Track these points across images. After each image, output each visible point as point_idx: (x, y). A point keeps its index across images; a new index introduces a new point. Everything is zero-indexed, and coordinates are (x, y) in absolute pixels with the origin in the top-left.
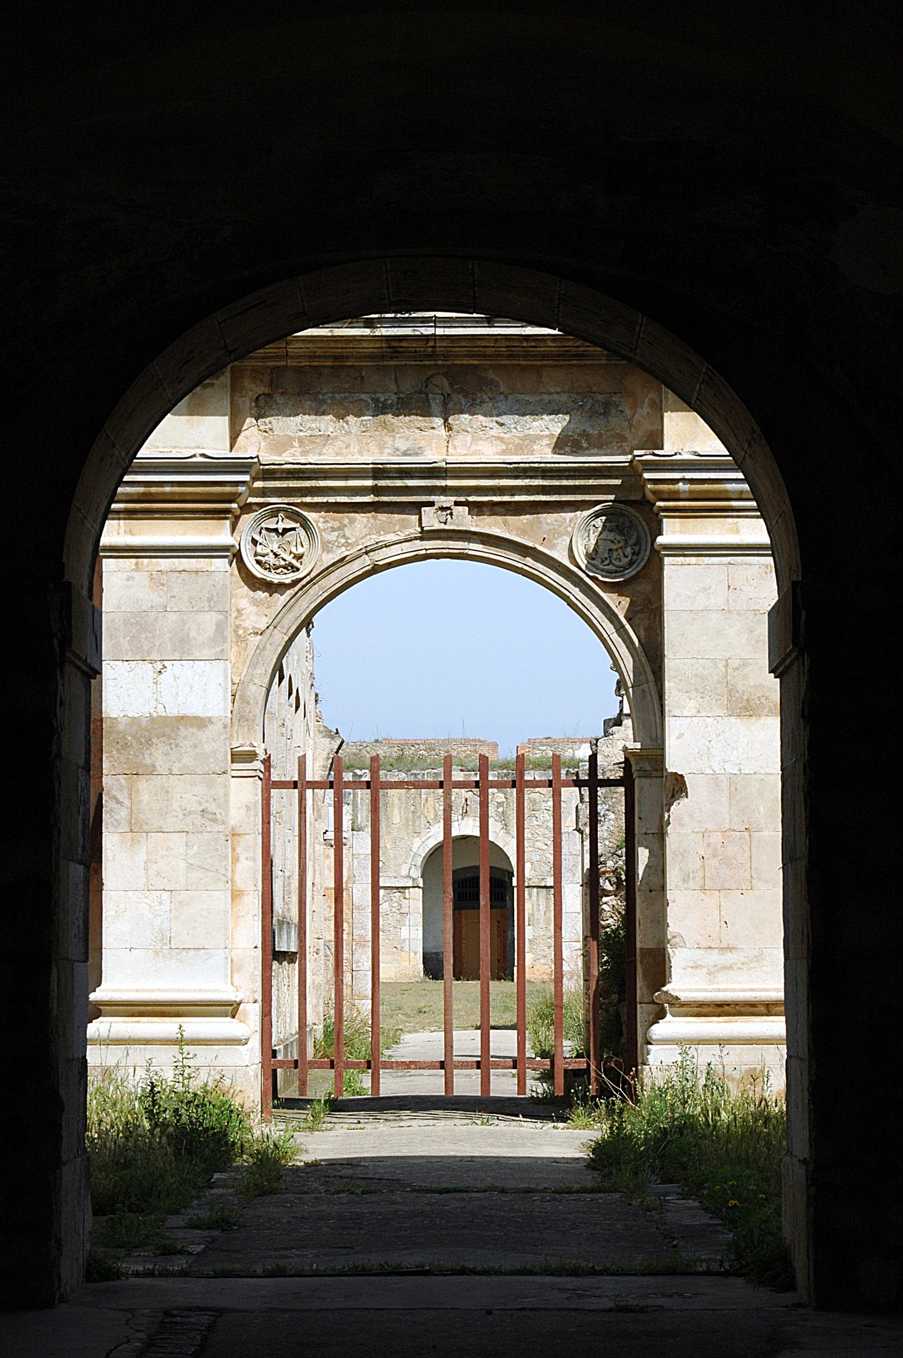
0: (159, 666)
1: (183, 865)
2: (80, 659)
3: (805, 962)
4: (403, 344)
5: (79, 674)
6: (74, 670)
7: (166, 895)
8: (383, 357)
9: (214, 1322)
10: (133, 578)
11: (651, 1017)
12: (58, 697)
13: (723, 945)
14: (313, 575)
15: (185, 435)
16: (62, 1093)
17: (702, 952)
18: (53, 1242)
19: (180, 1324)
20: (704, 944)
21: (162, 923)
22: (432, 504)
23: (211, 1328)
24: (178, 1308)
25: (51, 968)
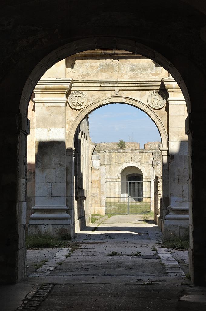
0: (49, 129)
1: (54, 176)
2: (24, 131)
3: (192, 203)
4: (107, 51)
5: (24, 135)
6: (22, 133)
7: (50, 184)
8: (102, 54)
9: (53, 287)
10: (43, 108)
11: (166, 213)
12: (18, 140)
13: (183, 196)
14: (85, 107)
15: (58, 71)
16: (19, 233)
17: (178, 198)
18: (16, 268)
19: (45, 287)
20: (179, 196)
21: (50, 190)
22: (114, 90)
23: (52, 288)
24: (46, 284)
25: (16, 204)
